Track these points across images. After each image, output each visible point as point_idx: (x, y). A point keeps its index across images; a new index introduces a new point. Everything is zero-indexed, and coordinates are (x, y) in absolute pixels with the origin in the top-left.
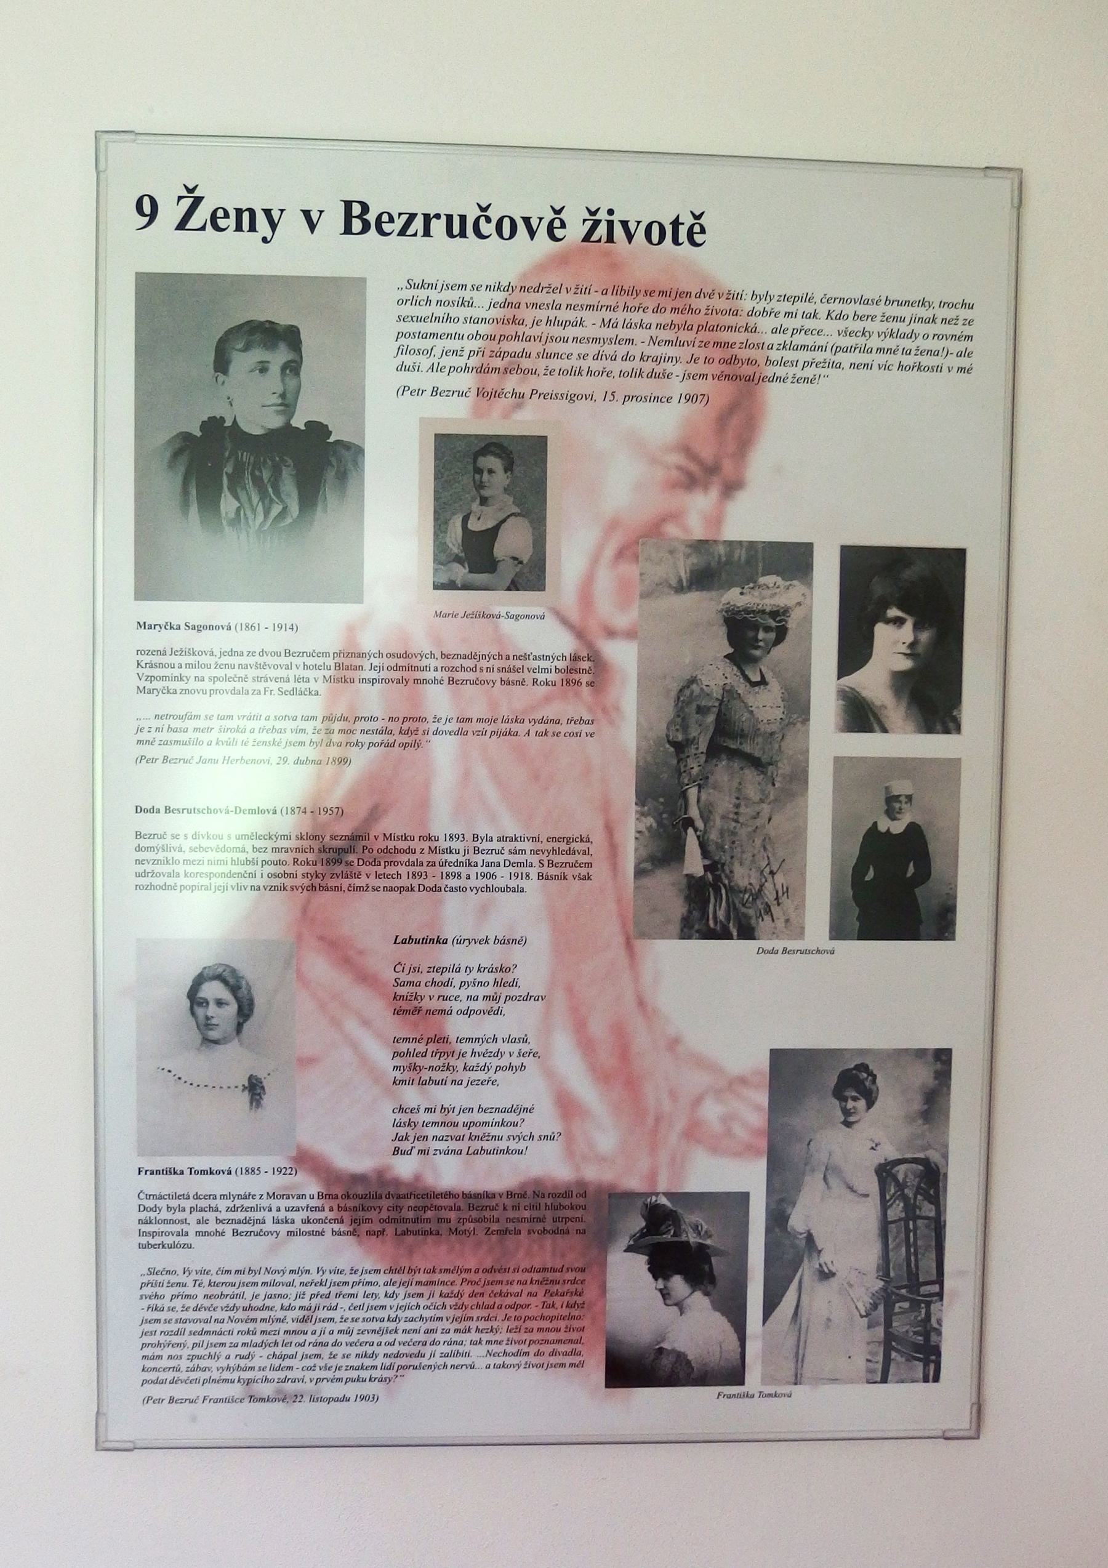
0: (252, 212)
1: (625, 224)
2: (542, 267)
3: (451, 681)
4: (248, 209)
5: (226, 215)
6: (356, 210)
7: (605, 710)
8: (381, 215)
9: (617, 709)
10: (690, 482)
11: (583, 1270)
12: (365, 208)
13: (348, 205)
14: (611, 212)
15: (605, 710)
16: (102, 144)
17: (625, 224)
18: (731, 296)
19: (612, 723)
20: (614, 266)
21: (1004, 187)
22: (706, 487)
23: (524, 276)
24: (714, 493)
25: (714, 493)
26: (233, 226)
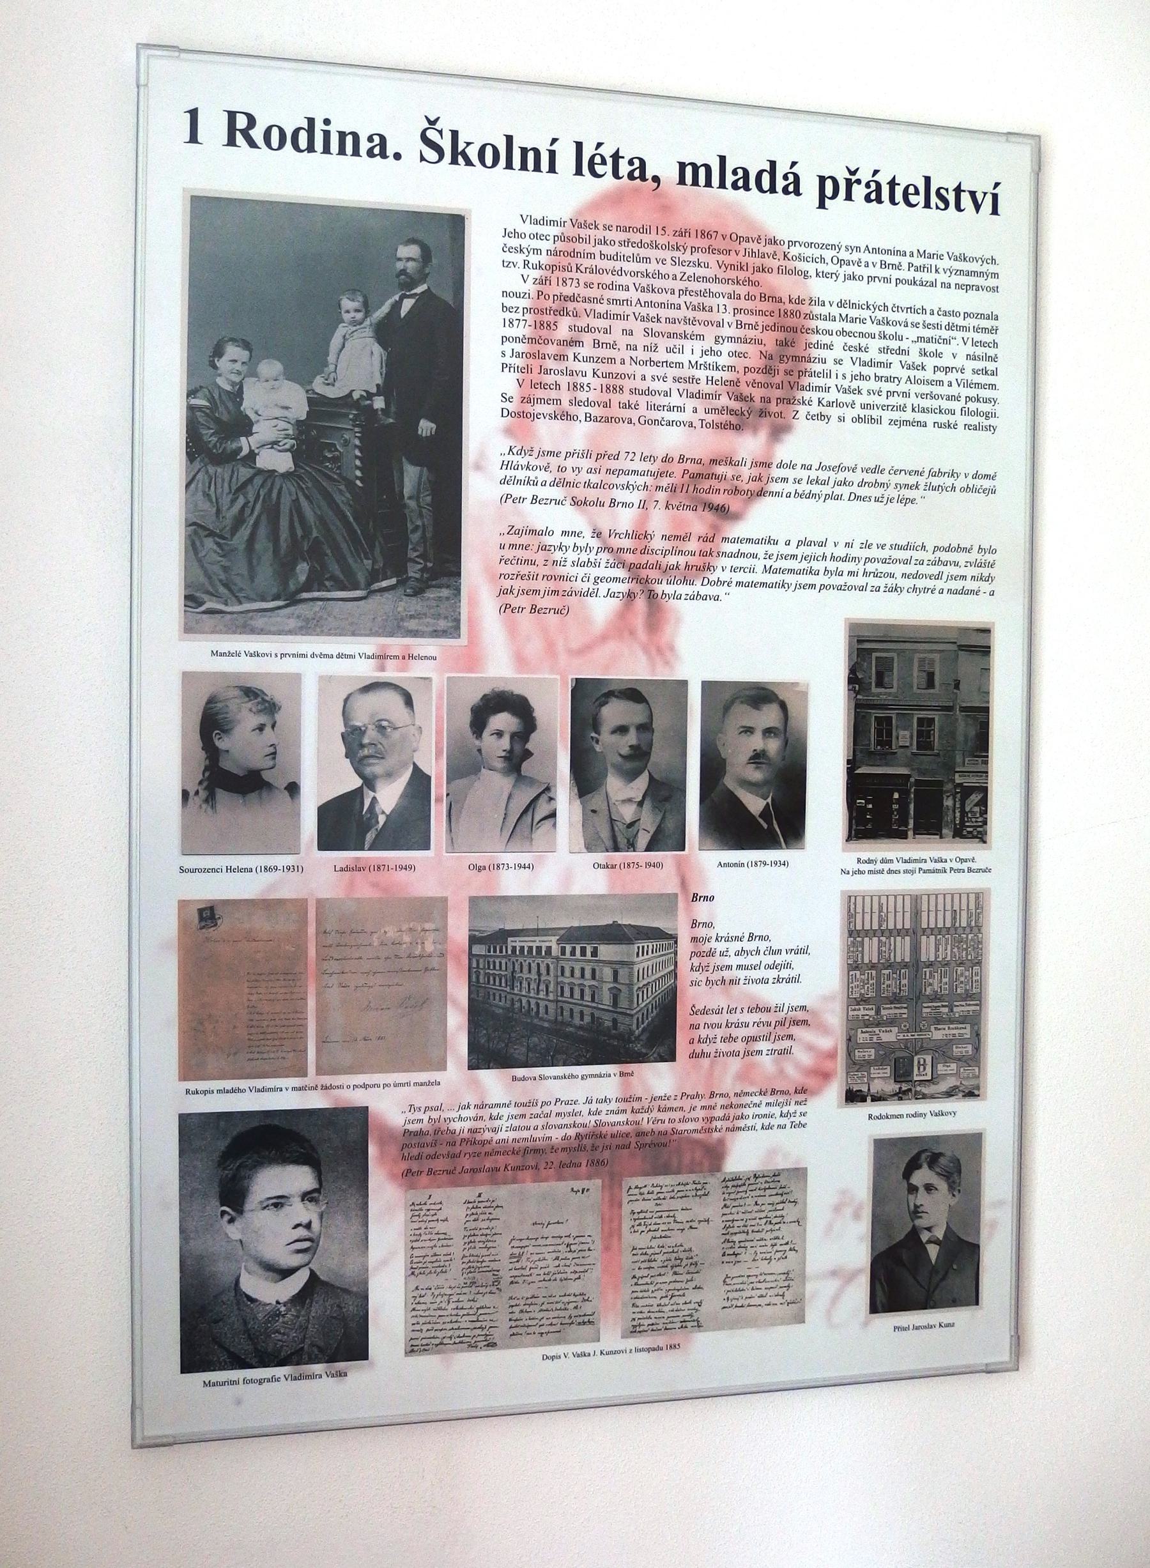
0: (356, 136)
1: (973, 194)
2: (597, 204)
3: (534, 609)
4: (533, 149)
5: (917, 192)
6: (241, 122)
7: (660, 651)
8: (907, 188)
9: (672, 648)
10: (737, 423)
11: (512, 1283)
12: (252, 121)
13: (232, 116)
14: (327, 122)
15: (660, 651)
16: (143, 60)
17: (973, 194)
18: (773, 242)
19: (667, 663)
20: (666, 208)
21: (144, 53)
22: (755, 430)
23: (580, 212)
24: (763, 435)
25: (763, 435)
26: (922, 204)
